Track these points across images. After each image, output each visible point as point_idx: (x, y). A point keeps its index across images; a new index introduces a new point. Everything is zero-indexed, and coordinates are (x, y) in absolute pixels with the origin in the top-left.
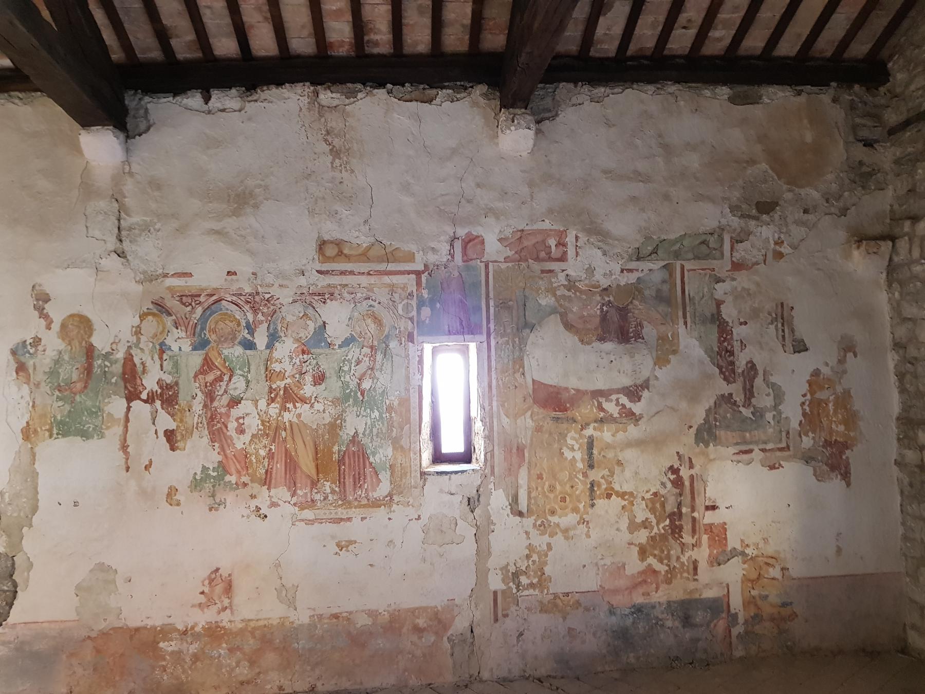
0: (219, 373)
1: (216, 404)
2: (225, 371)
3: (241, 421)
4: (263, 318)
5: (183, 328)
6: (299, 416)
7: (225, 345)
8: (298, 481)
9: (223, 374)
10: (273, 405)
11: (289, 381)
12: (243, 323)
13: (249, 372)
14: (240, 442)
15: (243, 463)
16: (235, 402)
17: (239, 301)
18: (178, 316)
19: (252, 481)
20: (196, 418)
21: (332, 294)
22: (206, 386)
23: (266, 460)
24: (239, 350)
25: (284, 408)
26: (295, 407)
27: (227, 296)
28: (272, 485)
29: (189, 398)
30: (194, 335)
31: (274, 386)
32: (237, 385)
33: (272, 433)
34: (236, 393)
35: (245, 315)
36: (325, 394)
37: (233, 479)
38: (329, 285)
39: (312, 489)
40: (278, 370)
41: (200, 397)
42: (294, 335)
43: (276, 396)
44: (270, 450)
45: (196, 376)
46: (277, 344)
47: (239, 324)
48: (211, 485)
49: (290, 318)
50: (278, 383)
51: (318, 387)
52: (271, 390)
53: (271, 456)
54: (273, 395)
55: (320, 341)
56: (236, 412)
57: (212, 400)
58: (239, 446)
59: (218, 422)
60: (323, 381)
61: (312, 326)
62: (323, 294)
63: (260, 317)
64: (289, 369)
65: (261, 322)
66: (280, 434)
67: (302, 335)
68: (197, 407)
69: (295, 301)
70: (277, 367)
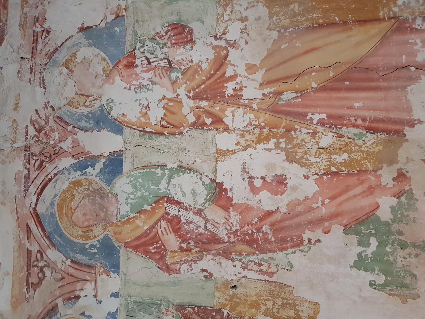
0: (163, 223)
1: (222, 233)
2: (160, 212)
3: (258, 183)
4: (69, 140)
5: (79, 286)
6: (251, 68)
7: (112, 209)
8: (394, 61)
9: (165, 216)
10: (227, 120)
11: (182, 91)
12: (76, 175)
13: (162, 166)
14: (303, 185)
15: (352, 181)
16: (219, 194)
17: (38, 182)
18: (57, 293)
19: (392, 161)
20: (251, 275)
21: (36, 20)
22: (189, 250)
23: (344, 131)
24: (122, 185)
25: (236, 98)
26: (233, 78)
27: (27, 202)
28: (404, 116)
29: (210, 285)
30: (90, 267)
31: (191, 119)
32: (187, 190)
33: (285, 121)
34: (203, 193)
35: (61, 172)
36: (210, 20)
37: (386, 205)
38: (22, 26)
39: (414, 31)
40: (161, 113)
41: (208, 263)
42: (99, 82)
43: (210, 114)
44: (321, 122)
45: (168, 270)
46: (114, 114)
47: (77, 184)
48: (401, 253)
49: (70, 91)
50: (186, 110)
51: (196, 35)
52: (199, 125)
53: (334, 122)
54: (209, 121)
55: (112, 35)
56: (239, 193)
57: (214, 239)
58: (310, 188)
59: (259, 230)
60: (184, 27)
61: (86, 52)
62: (35, 35)
63: (66, 145)
64: (161, 91)
65: (76, 144)
66: (288, 104)
67: (99, 69)
68: (226, 270)
69: (43, 83)
70: (156, 114)
